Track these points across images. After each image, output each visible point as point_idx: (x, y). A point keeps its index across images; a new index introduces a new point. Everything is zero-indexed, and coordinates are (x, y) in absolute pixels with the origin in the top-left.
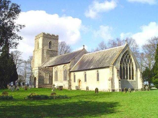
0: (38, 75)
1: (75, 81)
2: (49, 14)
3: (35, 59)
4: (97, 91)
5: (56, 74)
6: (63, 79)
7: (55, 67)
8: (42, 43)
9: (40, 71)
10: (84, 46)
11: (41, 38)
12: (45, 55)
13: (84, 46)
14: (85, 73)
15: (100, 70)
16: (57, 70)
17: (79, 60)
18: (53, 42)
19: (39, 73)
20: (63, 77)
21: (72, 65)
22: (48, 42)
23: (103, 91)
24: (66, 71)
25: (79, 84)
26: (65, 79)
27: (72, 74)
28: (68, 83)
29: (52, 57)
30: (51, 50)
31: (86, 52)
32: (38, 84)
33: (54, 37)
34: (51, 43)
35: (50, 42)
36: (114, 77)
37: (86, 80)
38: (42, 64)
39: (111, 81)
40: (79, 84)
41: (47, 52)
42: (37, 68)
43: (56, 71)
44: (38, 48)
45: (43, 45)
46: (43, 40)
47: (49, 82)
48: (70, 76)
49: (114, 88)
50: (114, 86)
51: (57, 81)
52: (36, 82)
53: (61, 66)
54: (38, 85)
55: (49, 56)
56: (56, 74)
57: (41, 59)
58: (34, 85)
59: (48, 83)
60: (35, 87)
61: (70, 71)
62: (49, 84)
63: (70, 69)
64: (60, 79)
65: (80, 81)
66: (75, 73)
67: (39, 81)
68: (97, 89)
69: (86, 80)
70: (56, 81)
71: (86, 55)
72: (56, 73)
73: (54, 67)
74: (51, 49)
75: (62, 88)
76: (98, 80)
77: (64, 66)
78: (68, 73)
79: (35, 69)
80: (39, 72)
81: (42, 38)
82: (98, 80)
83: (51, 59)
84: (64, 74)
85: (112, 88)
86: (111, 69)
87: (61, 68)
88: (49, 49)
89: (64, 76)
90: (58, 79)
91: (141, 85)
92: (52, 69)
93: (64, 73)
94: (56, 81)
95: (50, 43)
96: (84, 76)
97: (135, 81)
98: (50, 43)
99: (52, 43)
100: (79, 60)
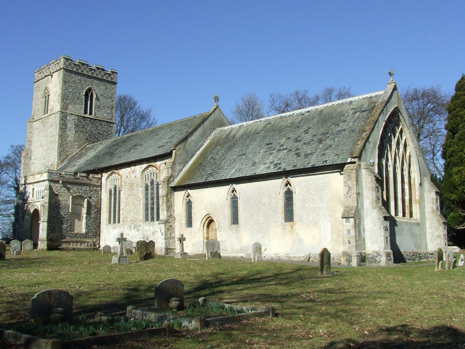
0: (47, 199)
1: (189, 223)
2: (50, 293)
3: (33, 148)
4: (325, 260)
5: (115, 199)
6: (141, 215)
7: (109, 173)
8: (60, 91)
9: (56, 188)
10: (217, 99)
11: (55, 75)
12: (71, 134)
13: (217, 99)
14: (234, 190)
15: (294, 181)
16: (118, 184)
17: (202, 149)
18: (98, 89)
19: (53, 196)
20: (142, 207)
21: (180, 164)
22: (83, 89)
23: (284, 258)
24: (152, 189)
25: (208, 233)
26: (112, 221)
27: (179, 197)
28: (163, 231)
29: (94, 142)
30: (90, 117)
31: (225, 120)
32: (48, 234)
33: (102, 73)
34: (92, 96)
35: (90, 90)
36: (362, 207)
37: (235, 220)
38: (58, 166)
39: (352, 220)
40: (205, 236)
41: (77, 126)
42: (45, 176)
43: (115, 188)
44: (46, 111)
45: (65, 98)
46: (65, 82)
47: (86, 228)
48: (170, 207)
49: (364, 249)
50: (364, 239)
51: (119, 222)
52: (41, 227)
53: (133, 168)
54: (47, 238)
55: (83, 140)
56: (115, 199)
57: (56, 146)
58: (187, 151)
59: (84, 231)
60: (35, 245)
61: (173, 184)
62: (86, 235)
63: (169, 180)
64: (130, 217)
65: (211, 221)
66: (190, 191)
67: (49, 222)
68: (326, 255)
69: (235, 220)
70: (115, 222)
71: (226, 130)
72: (115, 193)
73: (105, 175)
74: (91, 113)
75: (151, 249)
76: (289, 216)
77: (147, 168)
78: (162, 192)
79: (38, 178)
80: (51, 189)
81: (61, 76)
82: (289, 216)
83: (93, 147)
84: (147, 199)
85: (357, 247)
86: (354, 175)
87: (133, 175)
88: (86, 116)
89: (147, 205)
90: (121, 216)
91: (439, 236)
92: (101, 178)
93: (147, 194)
94: (153, 219)
95: (89, 94)
96: (229, 202)
97: (418, 224)
98: (89, 94)
99: (95, 96)
100: (201, 146)
